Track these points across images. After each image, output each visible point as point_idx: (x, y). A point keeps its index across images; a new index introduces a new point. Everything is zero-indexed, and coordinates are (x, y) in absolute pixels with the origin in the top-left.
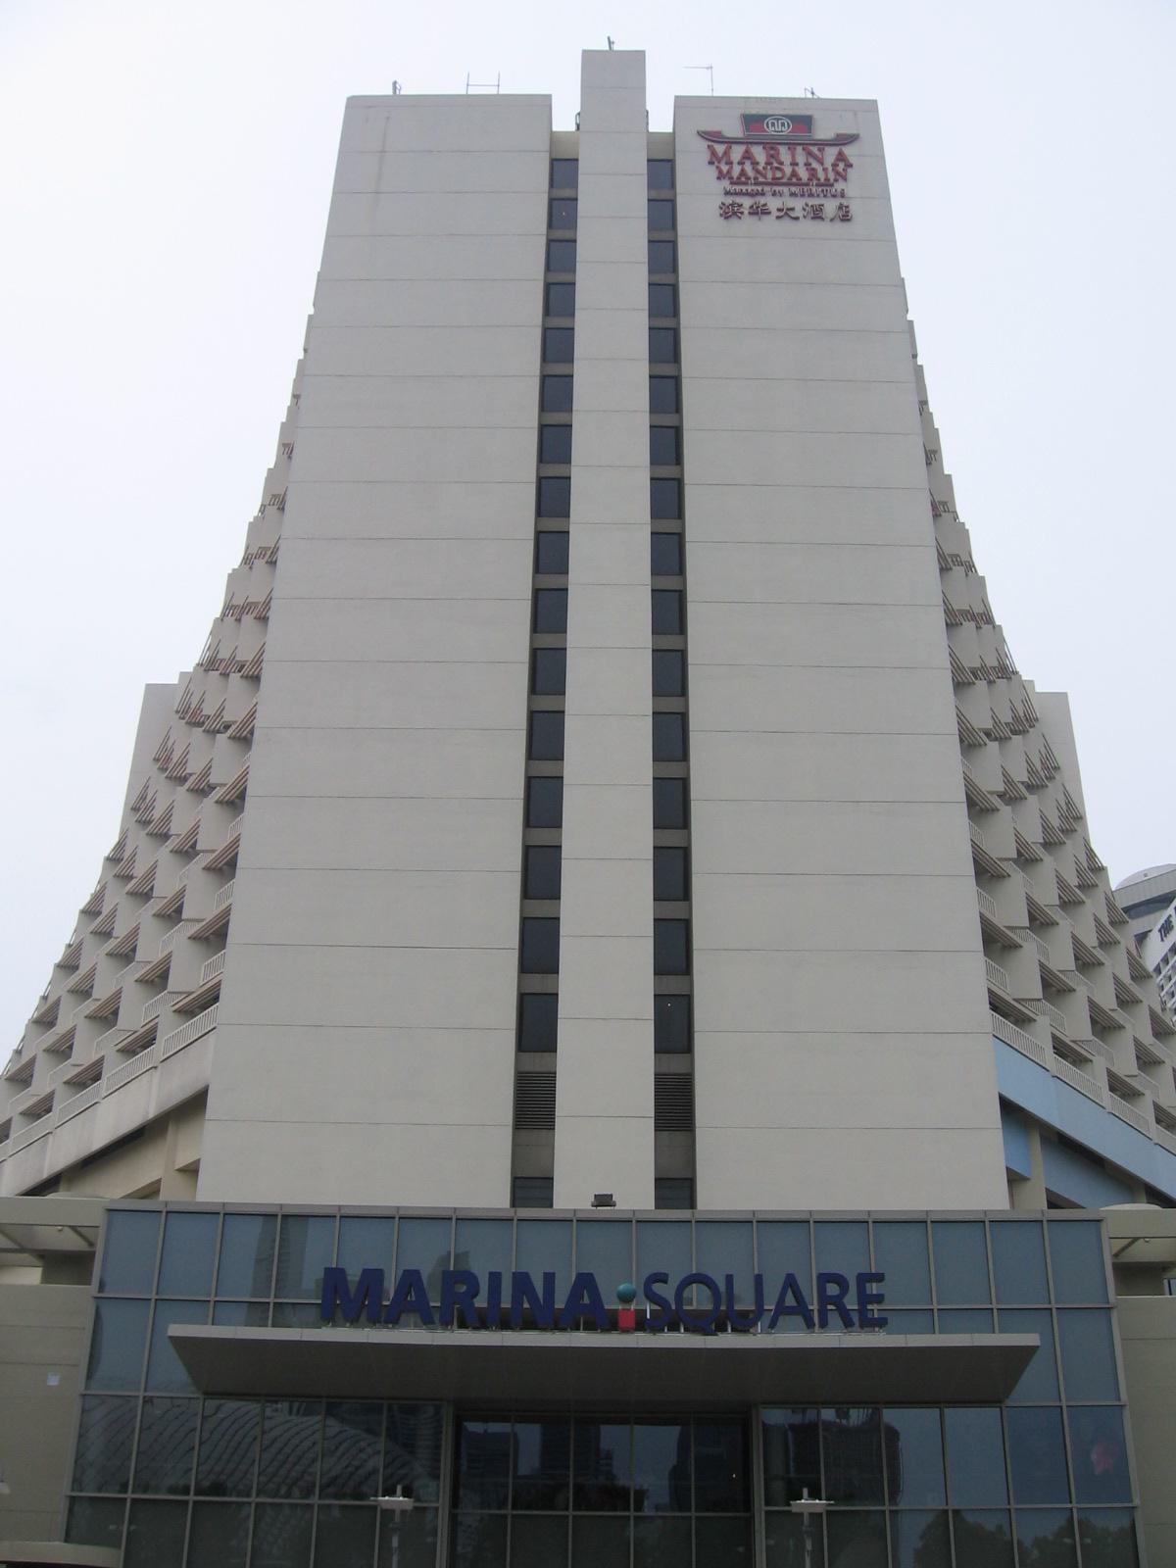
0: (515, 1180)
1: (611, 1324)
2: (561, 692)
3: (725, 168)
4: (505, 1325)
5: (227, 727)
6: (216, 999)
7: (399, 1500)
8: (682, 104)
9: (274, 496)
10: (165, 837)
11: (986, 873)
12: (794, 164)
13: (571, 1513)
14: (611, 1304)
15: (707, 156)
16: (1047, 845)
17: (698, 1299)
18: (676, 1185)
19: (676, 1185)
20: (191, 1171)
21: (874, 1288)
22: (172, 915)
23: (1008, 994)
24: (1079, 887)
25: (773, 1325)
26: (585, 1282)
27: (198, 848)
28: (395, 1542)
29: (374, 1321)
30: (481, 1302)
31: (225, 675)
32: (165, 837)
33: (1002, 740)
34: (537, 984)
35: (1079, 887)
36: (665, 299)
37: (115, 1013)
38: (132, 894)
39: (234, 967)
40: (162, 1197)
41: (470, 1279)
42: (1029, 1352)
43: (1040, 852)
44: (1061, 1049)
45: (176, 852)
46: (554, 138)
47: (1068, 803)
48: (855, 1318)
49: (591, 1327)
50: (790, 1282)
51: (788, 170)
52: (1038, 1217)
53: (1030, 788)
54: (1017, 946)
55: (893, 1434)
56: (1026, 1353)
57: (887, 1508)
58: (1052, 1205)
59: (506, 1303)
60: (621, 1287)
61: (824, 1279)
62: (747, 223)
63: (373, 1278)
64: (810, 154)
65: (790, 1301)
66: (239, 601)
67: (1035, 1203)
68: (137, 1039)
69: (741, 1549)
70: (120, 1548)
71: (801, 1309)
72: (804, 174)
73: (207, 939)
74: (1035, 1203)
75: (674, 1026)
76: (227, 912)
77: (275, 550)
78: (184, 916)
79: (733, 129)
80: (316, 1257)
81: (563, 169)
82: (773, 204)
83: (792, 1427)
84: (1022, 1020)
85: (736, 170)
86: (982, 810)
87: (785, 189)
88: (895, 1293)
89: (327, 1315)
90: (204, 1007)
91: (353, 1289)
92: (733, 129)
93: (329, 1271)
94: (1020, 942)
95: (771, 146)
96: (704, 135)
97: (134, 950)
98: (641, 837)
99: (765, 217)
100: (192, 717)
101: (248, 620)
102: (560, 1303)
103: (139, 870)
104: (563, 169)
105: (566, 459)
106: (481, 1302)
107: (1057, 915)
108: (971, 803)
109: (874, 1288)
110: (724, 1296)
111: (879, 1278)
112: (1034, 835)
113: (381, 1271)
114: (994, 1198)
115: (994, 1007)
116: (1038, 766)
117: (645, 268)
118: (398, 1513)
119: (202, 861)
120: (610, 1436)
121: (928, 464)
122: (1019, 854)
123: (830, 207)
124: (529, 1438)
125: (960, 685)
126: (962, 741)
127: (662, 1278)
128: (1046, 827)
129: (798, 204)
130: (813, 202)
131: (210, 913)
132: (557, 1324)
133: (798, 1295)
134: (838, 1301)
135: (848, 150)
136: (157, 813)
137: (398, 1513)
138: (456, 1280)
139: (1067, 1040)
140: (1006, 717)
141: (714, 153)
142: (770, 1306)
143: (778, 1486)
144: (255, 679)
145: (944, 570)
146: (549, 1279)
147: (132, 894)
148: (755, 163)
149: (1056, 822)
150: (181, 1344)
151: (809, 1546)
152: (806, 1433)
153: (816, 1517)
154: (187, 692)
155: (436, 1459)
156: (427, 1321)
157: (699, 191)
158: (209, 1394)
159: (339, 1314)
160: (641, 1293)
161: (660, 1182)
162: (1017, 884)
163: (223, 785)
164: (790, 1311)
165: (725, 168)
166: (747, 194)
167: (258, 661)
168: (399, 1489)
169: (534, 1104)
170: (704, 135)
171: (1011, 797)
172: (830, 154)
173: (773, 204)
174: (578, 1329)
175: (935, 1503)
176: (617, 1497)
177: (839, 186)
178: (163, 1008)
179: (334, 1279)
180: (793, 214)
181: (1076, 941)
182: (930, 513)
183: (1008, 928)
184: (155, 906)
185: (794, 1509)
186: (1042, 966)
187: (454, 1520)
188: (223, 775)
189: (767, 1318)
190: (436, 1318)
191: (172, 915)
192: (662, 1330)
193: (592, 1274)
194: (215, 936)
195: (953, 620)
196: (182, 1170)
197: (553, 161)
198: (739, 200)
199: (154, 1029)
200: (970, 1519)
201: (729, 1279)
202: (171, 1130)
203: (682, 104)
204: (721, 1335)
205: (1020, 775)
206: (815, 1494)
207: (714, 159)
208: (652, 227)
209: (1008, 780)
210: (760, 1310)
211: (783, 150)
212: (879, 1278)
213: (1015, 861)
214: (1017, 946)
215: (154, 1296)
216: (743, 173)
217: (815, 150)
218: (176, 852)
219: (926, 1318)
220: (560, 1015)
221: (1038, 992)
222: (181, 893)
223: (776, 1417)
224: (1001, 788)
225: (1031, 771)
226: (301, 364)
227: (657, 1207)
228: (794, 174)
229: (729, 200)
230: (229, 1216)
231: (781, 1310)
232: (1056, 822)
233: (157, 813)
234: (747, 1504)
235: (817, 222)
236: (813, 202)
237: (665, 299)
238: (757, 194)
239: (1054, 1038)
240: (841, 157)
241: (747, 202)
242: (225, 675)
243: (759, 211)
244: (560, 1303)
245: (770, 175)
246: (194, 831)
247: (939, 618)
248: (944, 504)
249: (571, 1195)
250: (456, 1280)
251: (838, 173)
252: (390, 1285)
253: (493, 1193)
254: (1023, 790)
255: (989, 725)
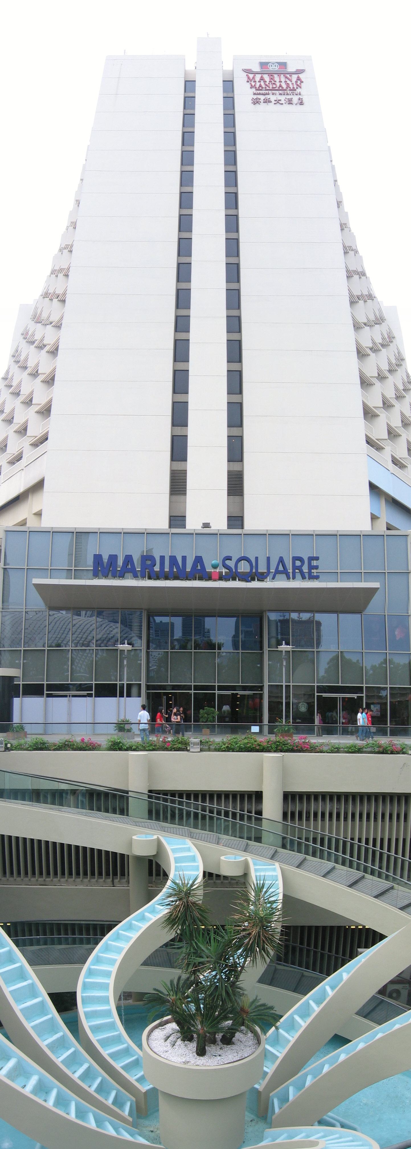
0: (170, 517)
1: (209, 577)
2: (189, 281)
3: (253, 84)
4: (167, 578)
5: (51, 323)
6: (47, 439)
7: (126, 647)
8: (236, 59)
9: (72, 222)
10: (25, 368)
11: (365, 383)
12: (280, 82)
13: (193, 651)
14: (209, 569)
15: (246, 79)
16: (390, 371)
17: (244, 567)
18: (236, 520)
19: (236, 520)
20: (39, 514)
21: (314, 563)
22: (28, 402)
23: (374, 437)
24: (404, 390)
25: (273, 578)
26: (199, 560)
27: (39, 372)
28: (125, 663)
29: (114, 577)
30: (157, 568)
31: (51, 300)
32: (25, 368)
33: (371, 326)
34: (179, 431)
35: (404, 390)
36: (230, 138)
37: (6, 446)
38: (12, 393)
39: (54, 425)
40: (28, 525)
41: (152, 558)
42: (375, 590)
43: (387, 374)
44: (395, 461)
45: (30, 374)
46: (186, 73)
47: (399, 353)
48: (307, 575)
49: (201, 579)
50: (281, 560)
51: (278, 84)
52: (383, 534)
53: (383, 345)
54: (378, 416)
55: (319, 624)
56: (374, 590)
57: (315, 650)
58: (388, 529)
59: (167, 569)
60: (213, 562)
61: (295, 559)
62: (263, 106)
63: (113, 558)
64: (286, 77)
65: (281, 568)
66: (57, 268)
67: (381, 528)
68: (15, 458)
69: (259, 665)
70: (20, 668)
71: (285, 572)
72: (284, 86)
73: (43, 412)
74: (381, 528)
75: (236, 451)
76: (50, 401)
77: (72, 246)
78: (33, 403)
79: (257, 68)
80: (92, 549)
81: (189, 85)
82: (273, 98)
83: (280, 621)
84: (379, 448)
85: (257, 86)
86: (363, 355)
87: (277, 92)
88: (323, 565)
89: (96, 575)
90: (42, 443)
91: (105, 564)
92: (257, 68)
93: (95, 556)
94: (379, 413)
95: (271, 74)
96: (245, 71)
97: (13, 418)
98: (222, 366)
99: (269, 104)
100: (37, 319)
101: (61, 275)
102: (188, 569)
103: (14, 383)
104: (189, 85)
105: (191, 207)
106: (157, 568)
107: (394, 402)
108: (358, 352)
109: (314, 563)
110: (254, 564)
111: (317, 559)
112: (385, 367)
113: (116, 555)
114: (364, 526)
115: (368, 442)
116: (386, 336)
117: (222, 125)
118: (126, 651)
119: (41, 378)
120: (209, 622)
121: (338, 207)
122: (379, 375)
123: (295, 99)
124: (178, 621)
125: (352, 303)
126: (354, 326)
127: (229, 558)
128: (390, 364)
129: (282, 98)
130: (289, 97)
131: (43, 401)
132: (187, 578)
133: (284, 566)
134: (300, 568)
135: (301, 76)
136: (22, 358)
137: (126, 651)
138: (147, 559)
139: (398, 458)
140: (372, 317)
141: (249, 78)
142: (273, 570)
143: (274, 641)
144: (63, 301)
145: (346, 253)
146: (184, 558)
147: (12, 393)
148: (265, 82)
149: (394, 361)
150: (38, 586)
151: (284, 664)
152: (284, 623)
153: (288, 652)
154: (36, 308)
155: (141, 631)
156: (135, 576)
157: (243, 93)
158: (51, 608)
159: (100, 574)
160: (221, 565)
161: (229, 518)
162: (378, 388)
163: (49, 344)
164: (281, 572)
165: (253, 84)
166: (262, 94)
167: (65, 294)
168: (126, 642)
169: (178, 485)
170: (245, 71)
171: (375, 350)
172: (294, 78)
173: (273, 98)
174: (196, 580)
175: (333, 648)
176: (211, 646)
177: (298, 90)
178: (25, 443)
179: (98, 558)
180: (280, 102)
181: (402, 413)
182: (339, 228)
183: (374, 407)
184: (21, 398)
185: (279, 649)
186: (388, 424)
187: (148, 653)
188: (50, 340)
189: (271, 575)
190: (139, 574)
191: (28, 402)
192: (229, 580)
193: (201, 557)
194: (46, 411)
195: (349, 275)
196: (35, 514)
197: (186, 81)
198: (259, 97)
199: (22, 453)
200: (347, 656)
201: (257, 558)
202: (30, 497)
203: (236, 59)
204: (253, 582)
205: (379, 340)
206: (287, 644)
207: (249, 80)
208: (225, 109)
209: (374, 343)
210: (269, 572)
211: (276, 76)
212: (317, 559)
213: (377, 378)
214: (378, 416)
215: (26, 567)
216: (260, 86)
217: (288, 76)
218: (30, 374)
219: (334, 575)
220: (189, 445)
221: (386, 436)
222: (32, 393)
223: (273, 616)
224: (371, 345)
225: (383, 339)
226: (84, 166)
227: (228, 528)
228: (280, 86)
229: (255, 97)
230: (55, 533)
231: (277, 572)
232: (394, 361)
233: (22, 358)
234: (261, 648)
235: (290, 105)
236: (289, 97)
237: (230, 138)
238: (266, 94)
239: (392, 456)
240: (299, 79)
241: (262, 97)
242: (51, 300)
243: (267, 101)
244: (188, 569)
245: (271, 86)
246: (37, 365)
247: (344, 274)
248: (345, 224)
249: (193, 524)
250: (147, 559)
251: (297, 85)
252: (120, 562)
253: (161, 522)
254: (380, 346)
255: (365, 321)
